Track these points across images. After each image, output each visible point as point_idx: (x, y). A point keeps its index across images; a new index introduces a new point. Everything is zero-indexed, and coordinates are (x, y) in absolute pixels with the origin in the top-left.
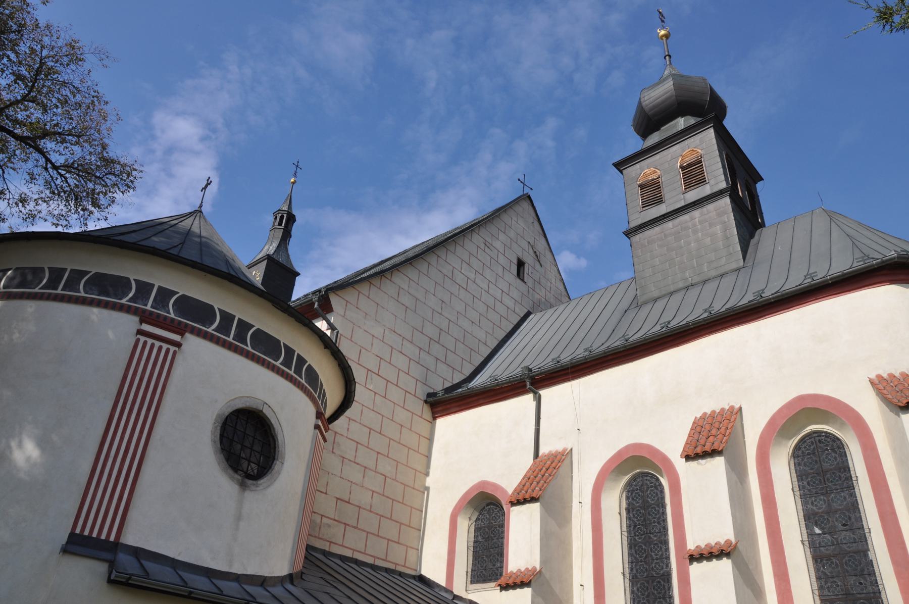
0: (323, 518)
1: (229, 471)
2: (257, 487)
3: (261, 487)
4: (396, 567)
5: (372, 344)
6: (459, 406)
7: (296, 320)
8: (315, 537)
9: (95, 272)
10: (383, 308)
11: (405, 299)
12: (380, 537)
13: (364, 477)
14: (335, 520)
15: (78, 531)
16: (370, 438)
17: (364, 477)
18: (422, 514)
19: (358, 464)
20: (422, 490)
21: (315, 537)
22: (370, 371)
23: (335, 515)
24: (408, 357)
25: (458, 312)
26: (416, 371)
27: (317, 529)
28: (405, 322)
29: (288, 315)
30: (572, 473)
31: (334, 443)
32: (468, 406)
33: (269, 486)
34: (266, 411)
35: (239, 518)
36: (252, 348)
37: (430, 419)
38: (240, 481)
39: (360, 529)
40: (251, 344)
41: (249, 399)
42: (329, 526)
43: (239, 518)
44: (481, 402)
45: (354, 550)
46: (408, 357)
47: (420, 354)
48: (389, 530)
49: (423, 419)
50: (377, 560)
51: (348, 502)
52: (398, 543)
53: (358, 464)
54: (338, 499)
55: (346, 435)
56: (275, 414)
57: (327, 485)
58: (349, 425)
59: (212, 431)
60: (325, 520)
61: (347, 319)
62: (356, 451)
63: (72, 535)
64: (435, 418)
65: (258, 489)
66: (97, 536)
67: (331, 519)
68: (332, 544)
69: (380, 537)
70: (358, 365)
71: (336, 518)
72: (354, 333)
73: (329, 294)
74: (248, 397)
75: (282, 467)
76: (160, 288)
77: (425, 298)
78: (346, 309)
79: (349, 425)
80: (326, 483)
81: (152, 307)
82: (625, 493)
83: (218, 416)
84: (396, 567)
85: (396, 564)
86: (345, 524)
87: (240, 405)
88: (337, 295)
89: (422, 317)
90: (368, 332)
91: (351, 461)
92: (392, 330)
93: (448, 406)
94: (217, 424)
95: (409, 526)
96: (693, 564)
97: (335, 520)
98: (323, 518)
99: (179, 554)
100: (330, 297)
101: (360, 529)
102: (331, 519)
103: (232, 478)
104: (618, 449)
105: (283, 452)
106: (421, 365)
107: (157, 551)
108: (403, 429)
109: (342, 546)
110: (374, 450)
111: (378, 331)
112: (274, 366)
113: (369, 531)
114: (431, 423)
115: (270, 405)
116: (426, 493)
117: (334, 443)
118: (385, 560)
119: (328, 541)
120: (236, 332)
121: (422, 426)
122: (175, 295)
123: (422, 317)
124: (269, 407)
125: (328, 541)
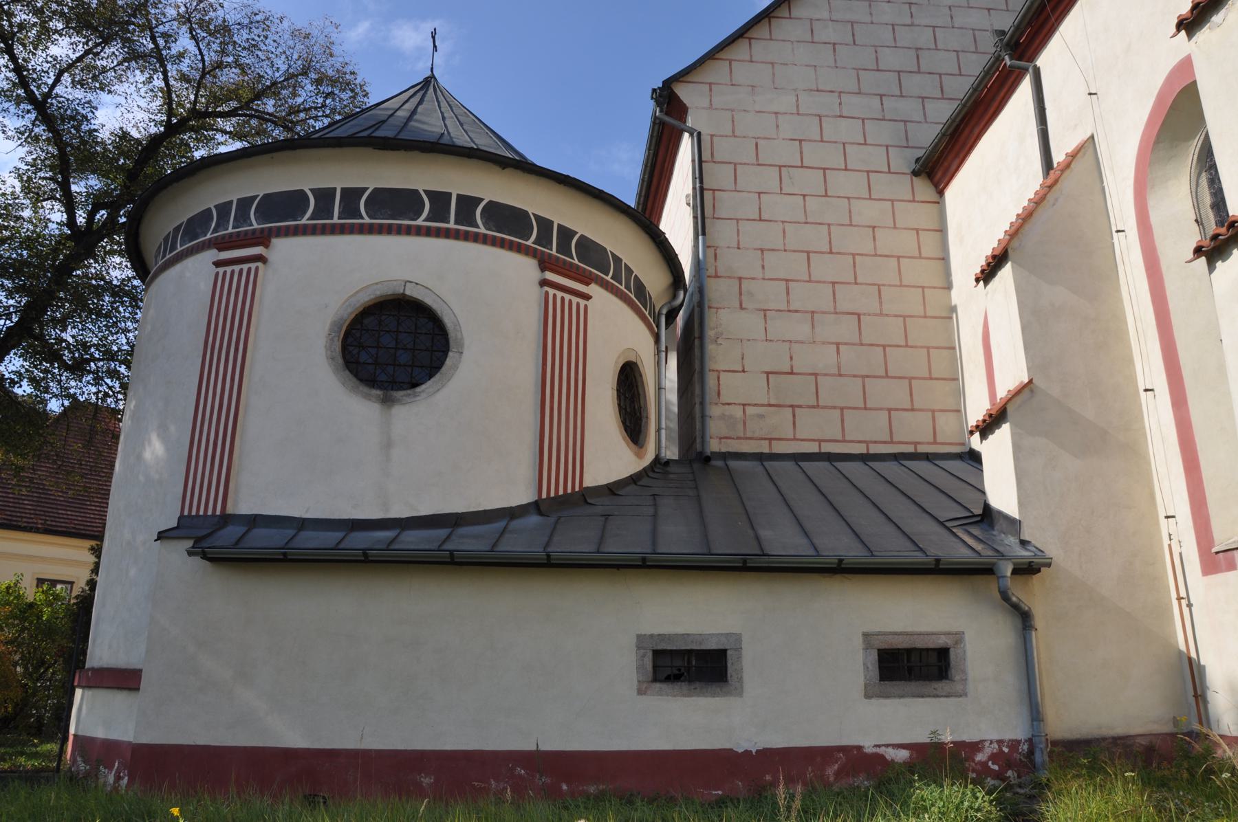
0: (747, 408)
1: (361, 388)
2: (415, 396)
3: (424, 395)
4: (916, 449)
5: (778, 126)
6: (957, 156)
7: (423, 152)
8: (738, 438)
9: (488, 200)
10: (787, 64)
11: (828, 33)
12: (870, 409)
13: (813, 327)
14: (770, 405)
15: (186, 513)
16: (812, 265)
17: (813, 327)
18: (956, 352)
19: (796, 311)
20: (944, 314)
21: (738, 438)
22: (785, 166)
23: (769, 398)
24: (859, 118)
25: (950, 7)
26: (882, 133)
27: (740, 426)
28: (837, 67)
29: (405, 150)
30: (1102, 182)
31: (741, 294)
32: (967, 149)
33: (439, 390)
34: (411, 292)
35: (388, 445)
36: (579, 261)
37: (935, 197)
38: (382, 396)
39: (825, 407)
40: (367, 213)
41: (379, 286)
42: (761, 416)
43: (388, 445)
44: (976, 131)
45: (820, 441)
46: (859, 118)
47: (882, 104)
48: (892, 394)
49: (918, 202)
50: (871, 446)
51: (792, 373)
52: (912, 410)
53: (796, 311)
54: (768, 373)
55: (761, 276)
56: (430, 290)
57: (743, 358)
58: (763, 260)
59: (326, 346)
60: (750, 410)
61: (716, 109)
62: (788, 293)
63: (181, 517)
64: (941, 193)
65: (418, 398)
66: (212, 513)
67: (763, 405)
68: (773, 442)
69: (870, 409)
70: (759, 167)
71: (772, 402)
72: (735, 123)
73: (673, 88)
74: (377, 284)
75: (460, 358)
76: (343, 190)
77: (871, 14)
78: (711, 96)
79: (763, 260)
80: (741, 356)
81: (339, 218)
82: (1204, 174)
83: (334, 324)
84: (916, 449)
85: (916, 444)
86: (792, 406)
87: (365, 298)
88: (689, 82)
89: (872, 46)
90: (764, 112)
91: (782, 311)
92: (811, 90)
93: (946, 164)
94: (334, 334)
95: (931, 378)
96: (1215, 268)
97: (770, 405)
98: (747, 408)
99: (307, 512)
100: (675, 91)
101: (825, 407)
102: (763, 405)
103: (367, 397)
104: (1156, 92)
105: (459, 337)
106: (890, 120)
107: (277, 514)
108: (878, 232)
109: (795, 439)
110: (824, 282)
111: (785, 102)
112: (334, 225)
113: (843, 405)
114: (938, 203)
115: (417, 282)
116: (954, 316)
117: (741, 294)
118: (892, 442)
119: (765, 439)
120: (341, 210)
121: (921, 215)
122: (366, 191)
123: (872, 46)
124: (417, 284)
125: (765, 439)
